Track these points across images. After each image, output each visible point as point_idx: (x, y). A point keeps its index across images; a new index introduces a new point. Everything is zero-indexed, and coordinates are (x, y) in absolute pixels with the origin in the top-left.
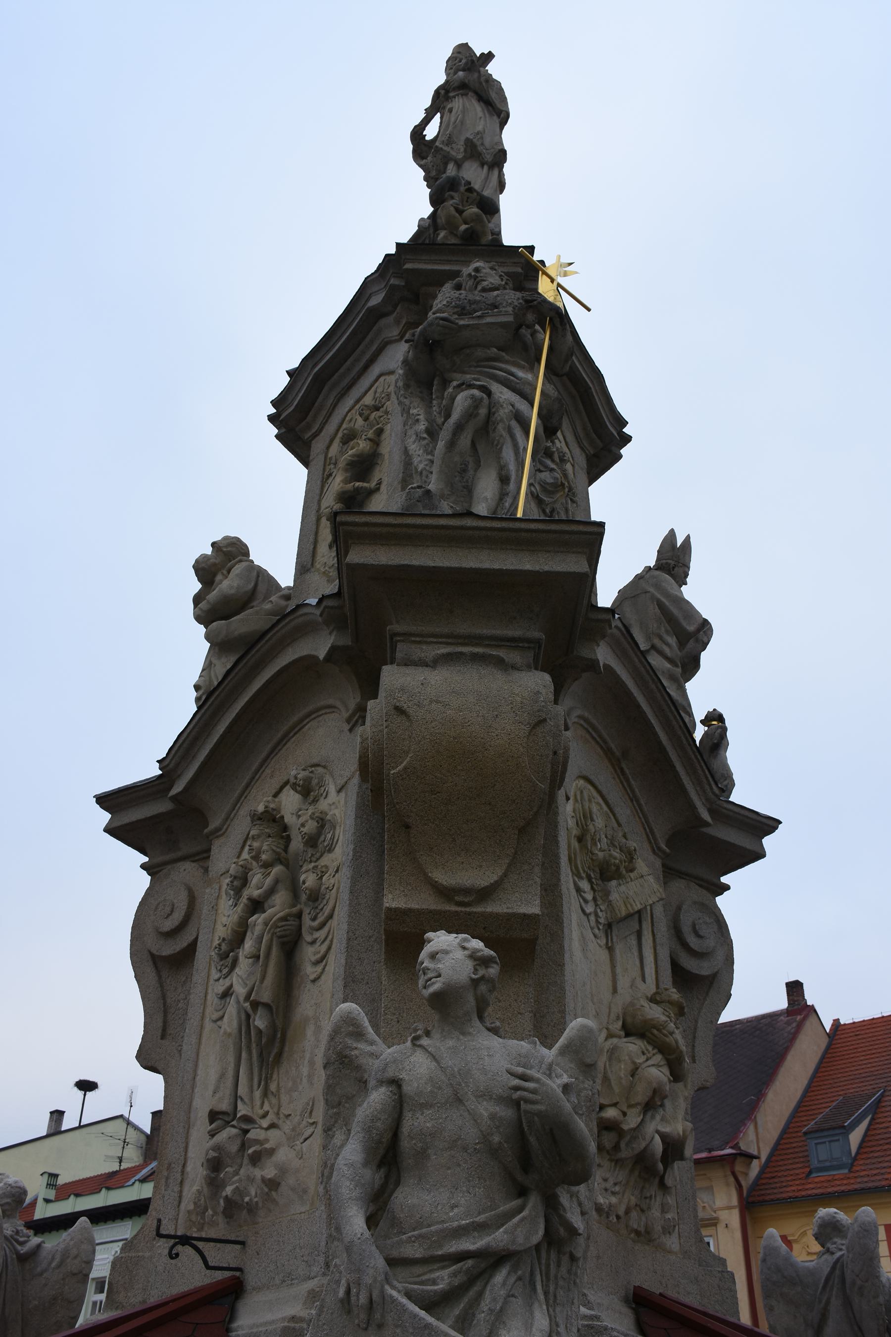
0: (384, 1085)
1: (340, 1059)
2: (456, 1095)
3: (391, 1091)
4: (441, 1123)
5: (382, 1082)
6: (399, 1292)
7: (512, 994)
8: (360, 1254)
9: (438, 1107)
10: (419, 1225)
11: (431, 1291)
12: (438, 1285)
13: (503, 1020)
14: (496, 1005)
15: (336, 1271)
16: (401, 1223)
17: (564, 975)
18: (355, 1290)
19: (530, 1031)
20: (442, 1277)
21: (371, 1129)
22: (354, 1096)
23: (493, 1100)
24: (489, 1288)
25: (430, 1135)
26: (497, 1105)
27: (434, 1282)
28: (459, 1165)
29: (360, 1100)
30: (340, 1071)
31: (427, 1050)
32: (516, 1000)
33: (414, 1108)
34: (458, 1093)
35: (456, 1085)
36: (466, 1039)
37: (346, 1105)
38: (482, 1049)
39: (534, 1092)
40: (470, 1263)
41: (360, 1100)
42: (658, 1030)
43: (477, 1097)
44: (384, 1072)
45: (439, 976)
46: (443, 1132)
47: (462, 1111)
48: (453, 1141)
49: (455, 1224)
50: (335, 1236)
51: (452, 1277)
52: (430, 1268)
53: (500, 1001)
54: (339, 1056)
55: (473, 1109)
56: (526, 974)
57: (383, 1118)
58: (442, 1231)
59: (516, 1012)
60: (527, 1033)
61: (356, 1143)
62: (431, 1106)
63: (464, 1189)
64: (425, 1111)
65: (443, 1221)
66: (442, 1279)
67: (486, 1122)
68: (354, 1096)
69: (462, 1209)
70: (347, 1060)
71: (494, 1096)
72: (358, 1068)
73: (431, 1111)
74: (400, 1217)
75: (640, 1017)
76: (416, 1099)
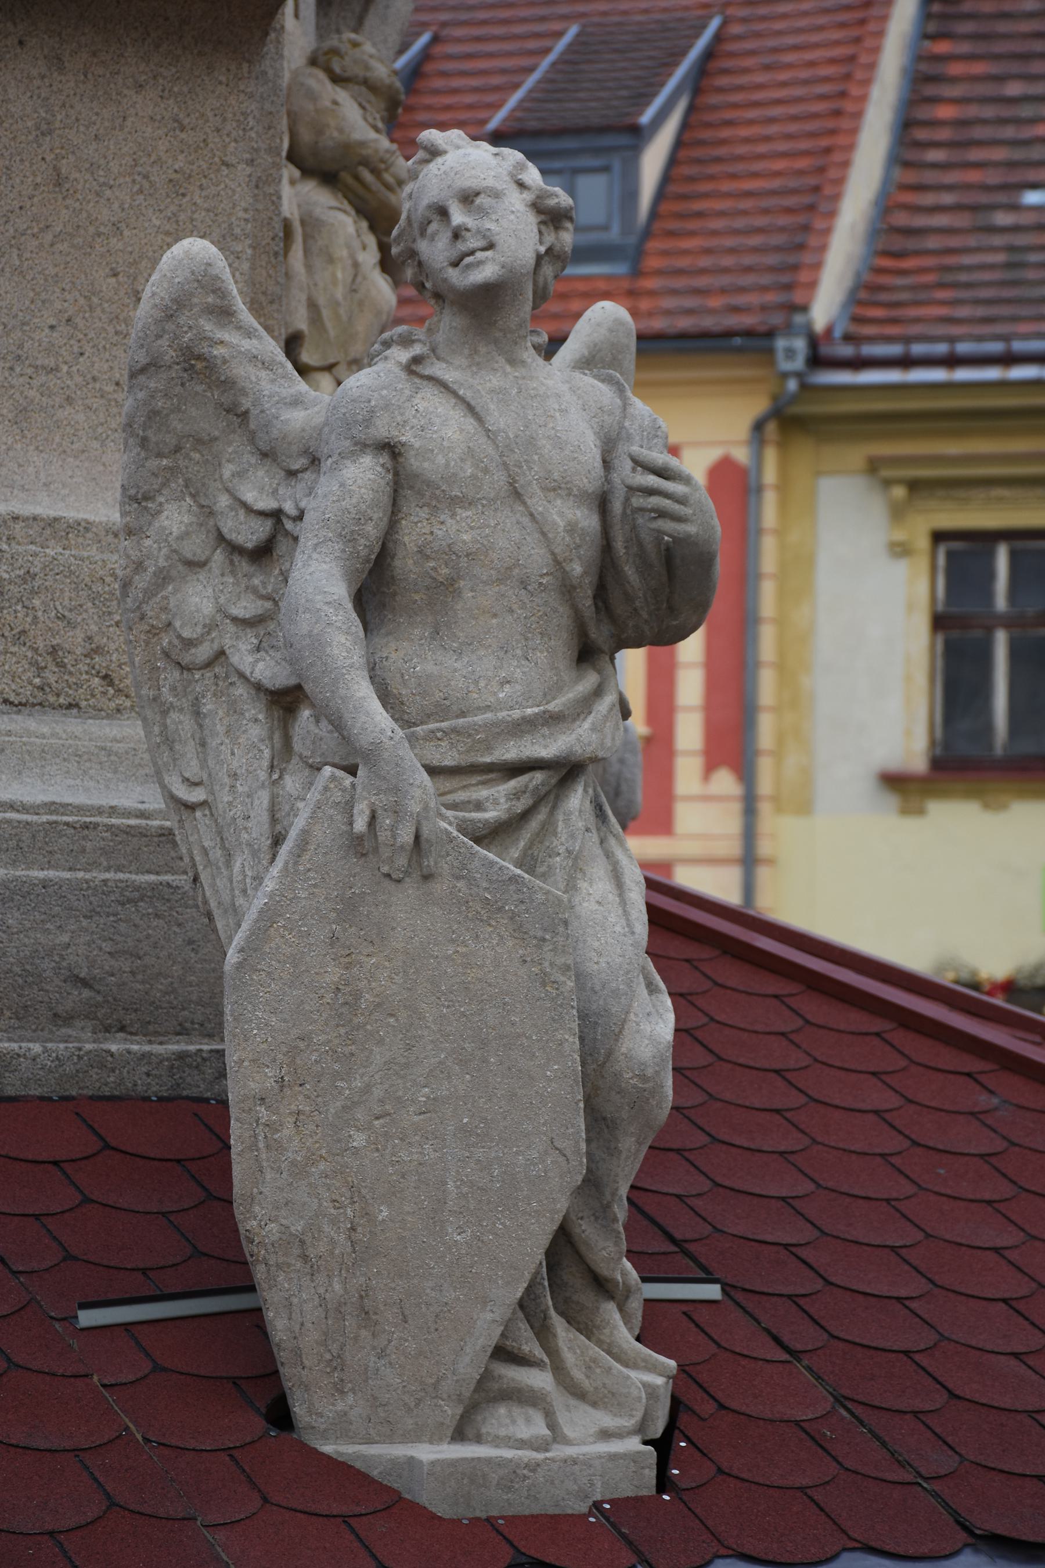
0: (368, 451)
1: (185, 361)
2: (511, 484)
3: (383, 465)
4: (487, 536)
5: (366, 446)
6: (450, 824)
7: (210, 114)
8: (397, 764)
9: (483, 506)
10: (441, 711)
11: (480, 821)
12: (485, 810)
13: (190, 176)
14: (175, 137)
15: (336, 787)
16: (402, 703)
17: (282, 57)
18: (388, 822)
19: (246, 210)
20: (494, 800)
21: (356, 536)
22: (216, 439)
23: (571, 498)
24: (560, 817)
25: (467, 555)
26: (578, 507)
27: (479, 806)
28: (511, 611)
29: (230, 450)
30: (183, 385)
31: (455, 394)
32: (218, 130)
33: (434, 503)
34: (515, 481)
35: (515, 465)
36: (517, 374)
37: (192, 454)
38: (548, 397)
39: (682, 501)
40: (538, 777)
41: (230, 450)
42: (376, 172)
43: (545, 489)
44: (367, 427)
45: (490, 246)
46: (490, 552)
47: (518, 515)
48: (507, 568)
49: (516, 714)
50: (171, 703)
51: (512, 800)
52: (465, 783)
53: (182, 129)
54: (184, 354)
55: (541, 513)
56: (245, 65)
57: (375, 516)
58: (495, 724)
59: (217, 159)
60: (241, 214)
61: (327, 559)
62: (470, 504)
63: (519, 652)
64: (459, 511)
65: (489, 706)
66: (496, 802)
67: (563, 539)
68: (216, 439)
69: (518, 687)
70: (199, 365)
71: (575, 491)
72: (228, 384)
73: (469, 513)
74: (400, 694)
75: (335, 134)
76: (444, 488)
